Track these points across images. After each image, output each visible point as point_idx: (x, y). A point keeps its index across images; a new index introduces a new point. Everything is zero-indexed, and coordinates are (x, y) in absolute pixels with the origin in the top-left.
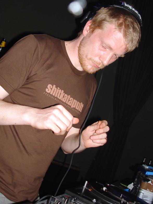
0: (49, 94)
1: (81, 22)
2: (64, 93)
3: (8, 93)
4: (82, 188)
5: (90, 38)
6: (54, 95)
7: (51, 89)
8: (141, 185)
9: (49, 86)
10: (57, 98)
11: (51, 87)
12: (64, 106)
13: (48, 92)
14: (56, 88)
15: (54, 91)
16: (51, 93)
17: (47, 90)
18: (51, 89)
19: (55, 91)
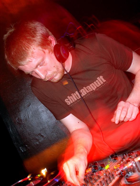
0: (71, 104)
6: (74, 101)
7: (69, 100)
14: (71, 97)
16: (72, 102)
18: (69, 100)
19: (72, 98)
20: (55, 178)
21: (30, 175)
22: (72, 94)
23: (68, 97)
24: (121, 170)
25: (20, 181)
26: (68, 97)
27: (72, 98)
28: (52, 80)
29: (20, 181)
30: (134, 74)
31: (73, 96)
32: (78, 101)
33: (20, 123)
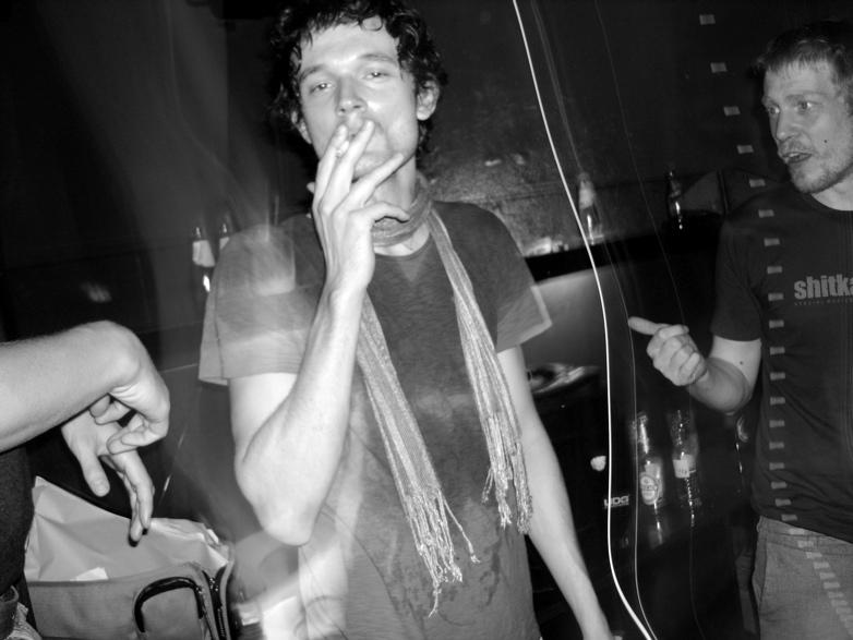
0: (807, 299)
1: (644, 419)
2: (846, 280)
3: (247, 626)
4: (193, 365)
5: (303, 57)
6: (818, 295)
7: (806, 288)
8: (307, 124)
9: (798, 286)
10: (830, 297)
11: (803, 284)
12: (145, 600)
13: (803, 297)
14: (817, 282)
15: (524, 462)
16: (811, 295)
17: (797, 296)
18: (806, 288)
19: (817, 287)
20: (484, 335)
21: (284, 598)
22: (823, 277)
23: (809, 279)
24: (347, 143)
25: (470, 545)
26: (809, 279)
27: (817, 287)
28: (816, 196)
29: (470, 545)
30: (520, 349)
31: (824, 282)
32: (829, 301)
33: (823, 57)
